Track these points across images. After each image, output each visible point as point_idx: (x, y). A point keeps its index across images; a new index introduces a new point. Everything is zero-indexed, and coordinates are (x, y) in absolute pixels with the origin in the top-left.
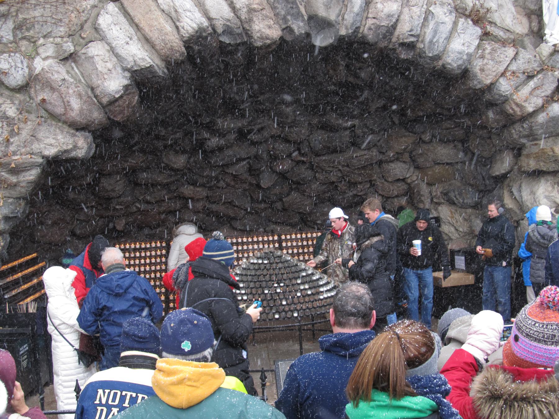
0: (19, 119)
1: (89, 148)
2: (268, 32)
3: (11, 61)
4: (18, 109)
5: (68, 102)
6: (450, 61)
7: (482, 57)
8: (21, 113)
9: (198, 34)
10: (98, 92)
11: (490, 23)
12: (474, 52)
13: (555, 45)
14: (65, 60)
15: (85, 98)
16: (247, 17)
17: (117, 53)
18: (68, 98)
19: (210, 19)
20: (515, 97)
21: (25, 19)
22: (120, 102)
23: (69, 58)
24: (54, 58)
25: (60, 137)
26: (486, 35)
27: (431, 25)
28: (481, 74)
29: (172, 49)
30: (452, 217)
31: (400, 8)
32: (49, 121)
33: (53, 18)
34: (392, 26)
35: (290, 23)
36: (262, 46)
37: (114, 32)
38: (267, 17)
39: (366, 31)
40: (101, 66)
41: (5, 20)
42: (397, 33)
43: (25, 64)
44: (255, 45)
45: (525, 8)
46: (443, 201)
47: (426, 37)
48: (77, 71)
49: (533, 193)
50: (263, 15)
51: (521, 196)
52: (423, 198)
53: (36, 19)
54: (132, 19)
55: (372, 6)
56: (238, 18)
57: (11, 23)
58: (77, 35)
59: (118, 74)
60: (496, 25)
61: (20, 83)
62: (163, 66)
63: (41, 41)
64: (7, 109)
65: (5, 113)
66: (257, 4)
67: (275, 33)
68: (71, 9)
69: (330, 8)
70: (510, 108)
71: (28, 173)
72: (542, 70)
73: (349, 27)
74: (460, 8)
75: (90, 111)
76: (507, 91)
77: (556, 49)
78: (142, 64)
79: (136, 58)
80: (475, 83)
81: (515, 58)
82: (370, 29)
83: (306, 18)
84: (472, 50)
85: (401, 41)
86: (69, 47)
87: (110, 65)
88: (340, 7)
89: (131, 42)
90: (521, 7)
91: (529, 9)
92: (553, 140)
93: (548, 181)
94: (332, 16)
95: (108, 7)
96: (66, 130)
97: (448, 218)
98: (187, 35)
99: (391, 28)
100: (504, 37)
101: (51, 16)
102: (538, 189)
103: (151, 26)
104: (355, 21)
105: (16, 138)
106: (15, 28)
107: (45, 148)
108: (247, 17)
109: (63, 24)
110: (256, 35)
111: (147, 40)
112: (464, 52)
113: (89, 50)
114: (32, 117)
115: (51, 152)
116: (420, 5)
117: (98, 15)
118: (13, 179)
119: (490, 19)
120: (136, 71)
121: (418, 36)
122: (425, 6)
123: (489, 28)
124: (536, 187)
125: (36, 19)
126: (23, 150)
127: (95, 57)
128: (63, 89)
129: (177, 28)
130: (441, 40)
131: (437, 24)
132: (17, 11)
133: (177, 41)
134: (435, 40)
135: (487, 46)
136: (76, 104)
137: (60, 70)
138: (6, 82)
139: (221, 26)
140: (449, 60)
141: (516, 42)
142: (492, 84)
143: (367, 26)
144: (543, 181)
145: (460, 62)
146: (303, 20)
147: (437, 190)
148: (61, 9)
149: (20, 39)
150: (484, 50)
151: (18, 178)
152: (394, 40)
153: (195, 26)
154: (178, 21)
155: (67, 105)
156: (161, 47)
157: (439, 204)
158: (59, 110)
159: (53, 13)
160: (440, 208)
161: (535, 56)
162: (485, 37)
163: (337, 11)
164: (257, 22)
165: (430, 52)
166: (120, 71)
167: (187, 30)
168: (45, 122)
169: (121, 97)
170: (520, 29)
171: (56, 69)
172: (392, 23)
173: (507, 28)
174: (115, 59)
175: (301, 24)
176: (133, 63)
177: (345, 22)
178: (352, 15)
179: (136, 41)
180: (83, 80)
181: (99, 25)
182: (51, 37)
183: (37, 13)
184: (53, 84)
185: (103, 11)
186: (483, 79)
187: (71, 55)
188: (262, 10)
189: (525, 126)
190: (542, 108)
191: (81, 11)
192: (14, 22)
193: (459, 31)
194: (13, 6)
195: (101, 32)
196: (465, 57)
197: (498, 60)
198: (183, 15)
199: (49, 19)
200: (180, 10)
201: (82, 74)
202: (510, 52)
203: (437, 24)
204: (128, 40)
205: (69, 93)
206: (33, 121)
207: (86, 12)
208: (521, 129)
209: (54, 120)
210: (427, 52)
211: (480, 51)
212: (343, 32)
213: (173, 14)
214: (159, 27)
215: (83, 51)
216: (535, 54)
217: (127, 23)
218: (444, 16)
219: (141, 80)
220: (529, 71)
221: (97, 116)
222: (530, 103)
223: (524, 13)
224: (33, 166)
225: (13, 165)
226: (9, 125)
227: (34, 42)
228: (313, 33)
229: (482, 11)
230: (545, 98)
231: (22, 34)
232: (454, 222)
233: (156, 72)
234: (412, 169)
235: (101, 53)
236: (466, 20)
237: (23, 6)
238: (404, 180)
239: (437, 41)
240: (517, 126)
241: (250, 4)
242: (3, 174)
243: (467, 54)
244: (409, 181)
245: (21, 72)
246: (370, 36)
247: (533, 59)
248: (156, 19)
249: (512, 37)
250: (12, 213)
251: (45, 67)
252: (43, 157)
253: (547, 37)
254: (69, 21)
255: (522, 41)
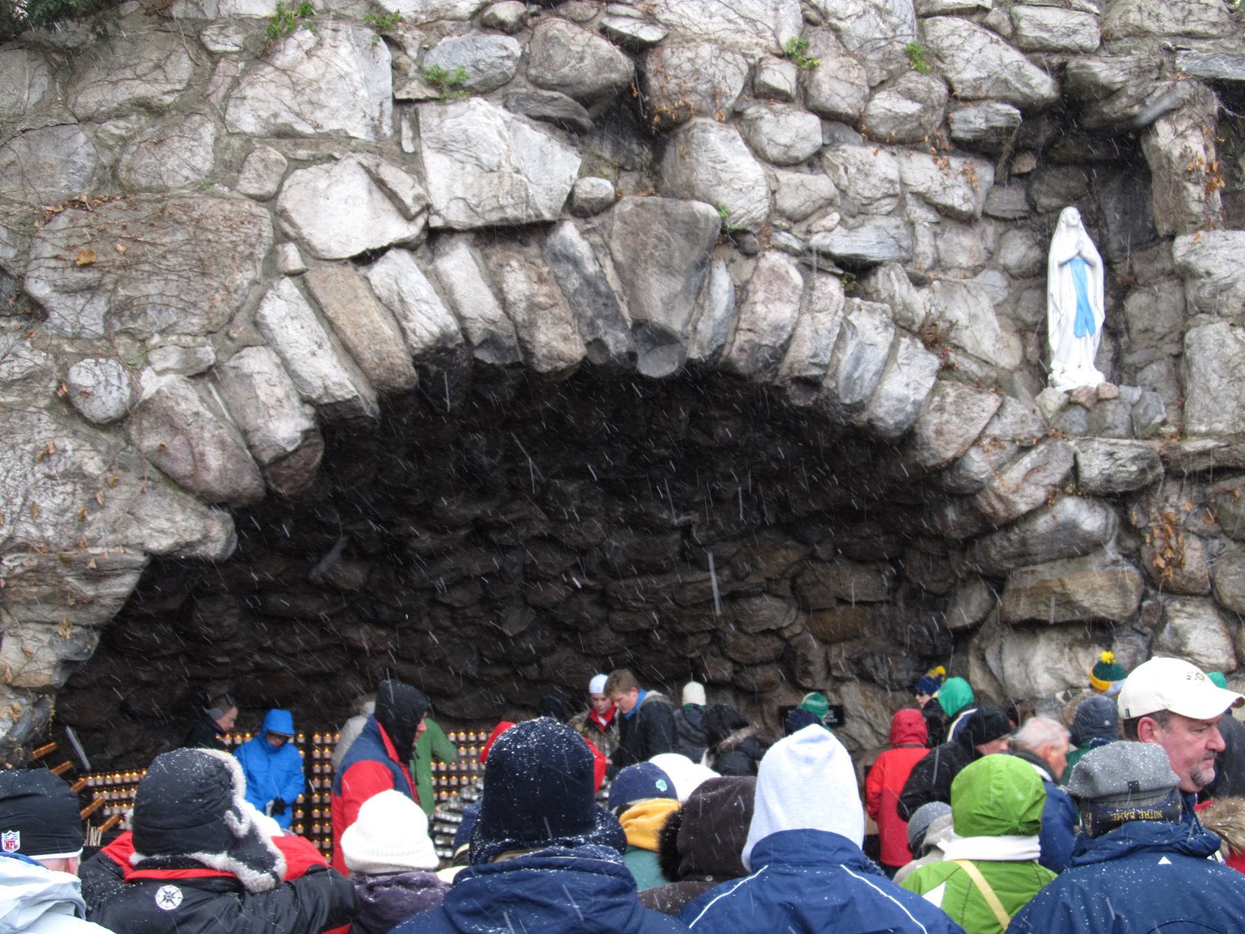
0: (106, 480)
1: (229, 542)
2: (561, 346)
3: (98, 372)
4: (104, 462)
5: (202, 454)
6: (882, 415)
7: (941, 409)
8: (110, 470)
9: (439, 345)
10: (256, 439)
11: (956, 347)
12: (926, 400)
13: (1069, 392)
14: (199, 376)
15: (230, 450)
16: (526, 318)
17: (294, 371)
18: (201, 448)
19: (460, 318)
20: (996, 484)
21: (129, 297)
22: (292, 461)
23: (204, 375)
24: (177, 372)
25: (179, 518)
26: (947, 370)
27: (851, 347)
28: (937, 439)
29: (391, 369)
30: (866, 707)
31: (796, 315)
32: (161, 487)
33: (181, 300)
34: (782, 346)
35: (601, 333)
36: (549, 372)
37: (291, 331)
38: (561, 319)
39: (734, 354)
40: (263, 392)
41: (92, 298)
42: (789, 358)
43: (125, 381)
44: (539, 370)
45: (1017, 319)
46: (850, 675)
47: (841, 368)
48: (217, 398)
49: (1024, 663)
50: (554, 315)
51: (1002, 668)
52: (811, 668)
53: (151, 300)
54: (322, 310)
55: (746, 308)
56: (509, 318)
57: (103, 303)
58: (222, 333)
59: (293, 408)
60: (965, 351)
61: (112, 413)
62: (374, 398)
63: (156, 339)
64: (86, 460)
65: (80, 468)
66: (546, 295)
67: (575, 350)
68: (215, 284)
69: (673, 308)
70: (986, 504)
71: (116, 581)
72: (1046, 436)
73: (705, 344)
74: (903, 319)
75: (239, 473)
76: (983, 473)
77: (1072, 399)
78: (338, 393)
79: (328, 382)
80: (926, 455)
81: (998, 414)
82: (742, 350)
83: (629, 324)
84: (922, 395)
85: (796, 374)
86: (208, 354)
87: (279, 392)
88: (690, 308)
89: (320, 352)
90: (1008, 316)
91: (1024, 321)
92: (1063, 565)
93: (1052, 640)
94: (676, 325)
95: (281, 287)
96: (191, 505)
97: (860, 708)
98: (421, 346)
99: (780, 351)
100: (980, 374)
101: (177, 296)
102: (1033, 655)
103: (357, 325)
104: (715, 335)
105: (99, 515)
106: (108, 312)
107: (151, 536)
108: (526, 318)
109: (198, 312)
110: (540, 352)
111: (349, 352)
112: (908, 398)
113: (245, 361)
114: (131, 477)
115: (160, 544)
116: (832, 309)
117: (262, 297)
118: (89, 591)
119: (955, 341)
120: (326, 405)
121: (825, 367)
122: (840, 313)
123: (953, 357)
124: (1031, 651)
125: (151, 300)
126: (111, 537)
127: (255, 376)
128: (194, 430)
129: (403, 331)
130: (868, 376)
131: (861, 346)
132: (116, 282)
133: (402, 355)
134: (856, 375)
135: (949, 390)
136: (214, 459)
137: (190, 395)
138: (86, 413)
139: (479, 332)
140: (880, 412)
141: (1001, 385)
142: (955, 459)
143: (737, 343)
144: (1042, 640)
145: (900, 417)
146: (625, 329)
147: (840, 655)
148: (198, 284)
149: (117, 334)
150: (943, 397)
151: (97, 589)
152: (784, 370)
153: (435, 330)
154: (406, 318)
155: (198, 460)
156: (374, 365)
157: (842, 680)
158: (182, 467)
159: (181, 291)
160: (844, 689)
161: (1034, 411)
162: (946, 374)
163: (684, 315)
164: (543, 329)
165: (846, 397)
166: (297, 404)
167: (421, 337)
168: (154, 488)
169: (296, 451)
170: (1007, 360)
171: (182, 392)
172: (781, 342)
173: (985, 358)
174: (288, 381)
175: (622, 336)
176: (321, 391)
177: (698, 336)
178: (711, 323)
179: (330, 352)
180: (228, 417)
181: (263, 317)
182: (173, 333)
183: (153, 288)
184: (176, 420)
185: (271, 291)
186: (941, 449)
187: (210, 367)
188: (552, 306)
189: (1013, 537)
190: (1045, 506)
191: (232, 289)
192: (109, 301)
193: (900, 361)
194: (109, 272)
195: (266, 331)
196: (909, 408)
197: (968, 416)
198: (413, 309)
199: (174, 300)
200: (409, 300)
201: (227, 404)
202: (990, 402)
203: (861, 346)
204: (315, 347)
205: (202, 438)
206: (133, 486)
207: (240, 292)
208: (1006, 544)
209: (170, 485)
210: (841, 396)
211: (937, 399)
212: (694, 353)
213: (397, 306)
214: (370, 328)
215: (232, 363)
216: (1034, 406)
217: (313, 316)
218: (874, 332)
219: (332, 422)
220: (1022, 437)
221: (249, 482)
222: (1022, 496)
223: (1014, 329)
224: (128, 568)
225: (92, 565)
226: (87, 488)
227: (143, 341)
228: (641, 353)
229: (942, 325)
230: (1051, 488)
231: (122, 324)
232: (871, 716)
233: (361, 409)
234: (793, 612)
235: (265, 369)
236: (912, 340)
237: (127, 274)
238: (777, 633)
239: (861, 377)
240: (997, 538)
241: (533, 295)
242: (70, 579)
243: (914, 403)
244: (787, 634)
245: (115, 394)
246: (742, 363)
247: (1030, 416)
248: (367, 314)
249: (994, 374)
250: (77, 654)
251: (164, 389)
252: (146, 553)
253: (1055, 376)
254: (211, 307)
255: (1011, 382)
